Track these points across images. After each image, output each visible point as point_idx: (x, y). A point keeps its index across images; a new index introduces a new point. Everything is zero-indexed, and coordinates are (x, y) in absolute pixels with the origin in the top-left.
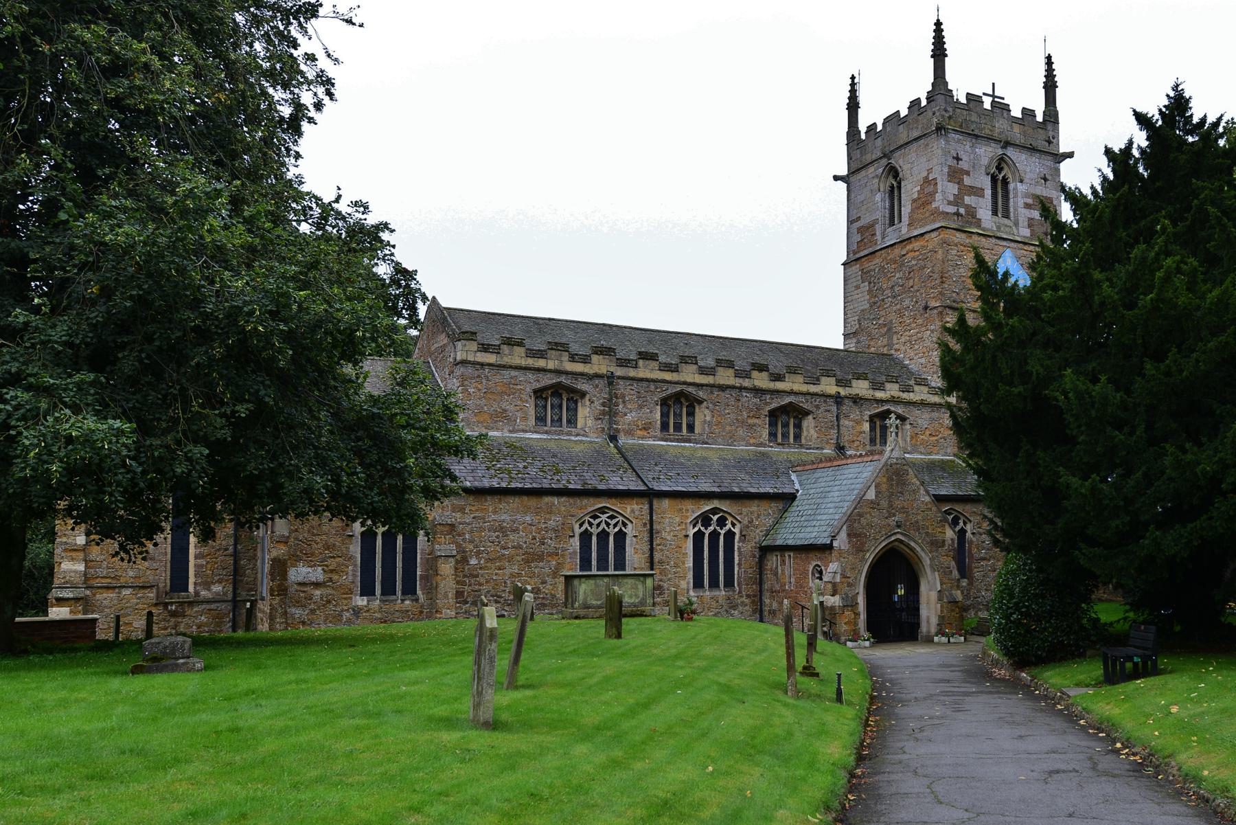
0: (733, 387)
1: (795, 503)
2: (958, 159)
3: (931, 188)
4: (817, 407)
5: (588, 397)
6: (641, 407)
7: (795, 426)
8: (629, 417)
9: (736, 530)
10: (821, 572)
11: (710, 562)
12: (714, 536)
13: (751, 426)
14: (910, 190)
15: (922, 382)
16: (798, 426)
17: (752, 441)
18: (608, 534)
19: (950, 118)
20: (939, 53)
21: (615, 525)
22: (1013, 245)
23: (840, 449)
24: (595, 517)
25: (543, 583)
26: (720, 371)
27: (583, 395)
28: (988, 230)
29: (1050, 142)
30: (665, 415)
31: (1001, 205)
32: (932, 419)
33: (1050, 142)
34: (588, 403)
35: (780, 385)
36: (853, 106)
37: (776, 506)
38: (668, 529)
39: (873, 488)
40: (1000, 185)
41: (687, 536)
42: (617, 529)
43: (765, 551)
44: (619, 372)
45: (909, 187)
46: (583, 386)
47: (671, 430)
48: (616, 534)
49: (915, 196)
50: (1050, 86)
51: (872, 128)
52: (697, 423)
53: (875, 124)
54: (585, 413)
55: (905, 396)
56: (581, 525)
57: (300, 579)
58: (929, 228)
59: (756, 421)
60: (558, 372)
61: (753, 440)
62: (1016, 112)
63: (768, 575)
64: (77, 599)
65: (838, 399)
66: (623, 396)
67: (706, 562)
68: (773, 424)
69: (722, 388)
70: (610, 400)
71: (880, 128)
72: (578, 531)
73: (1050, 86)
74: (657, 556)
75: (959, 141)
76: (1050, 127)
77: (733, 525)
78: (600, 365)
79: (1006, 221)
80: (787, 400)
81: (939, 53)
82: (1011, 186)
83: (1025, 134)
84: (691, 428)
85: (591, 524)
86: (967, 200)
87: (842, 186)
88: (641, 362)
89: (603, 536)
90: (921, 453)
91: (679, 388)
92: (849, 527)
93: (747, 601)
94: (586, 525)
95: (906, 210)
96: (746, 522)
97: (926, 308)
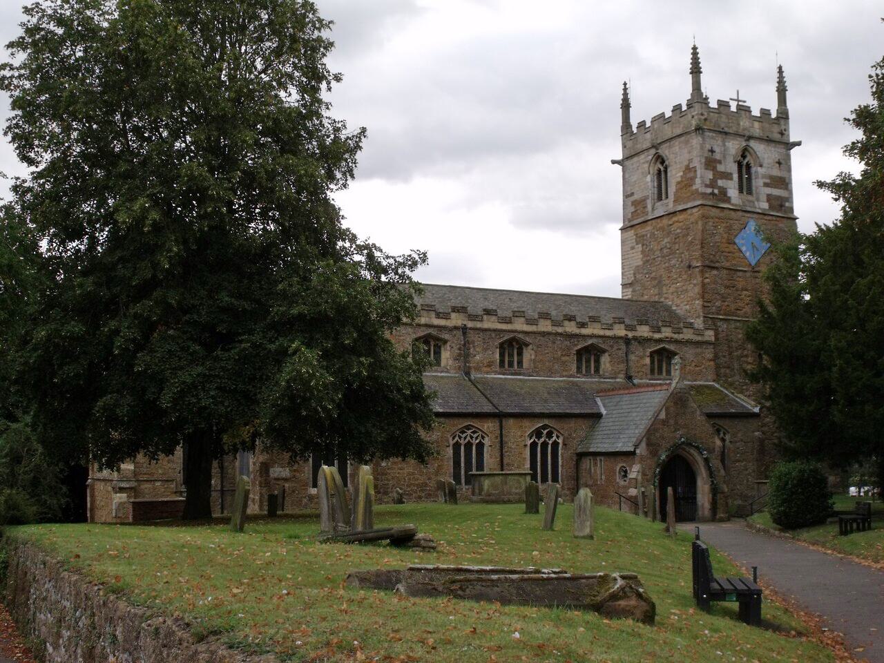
0: (549, 334)
1: (602, 421)
2: (712, 151)
3: (692, 174)
4: (612, 347)
5: (449, 344)
6: (485, 350)
7: (595, 361)
8: (478, 357)
9: (560, 441)
10: (626, 472)
11: (541, 465)
12: (545, 445)
13: (564, 363)
14: (675, 175)
15: (690, 326)
16: (597, 362)
17: (565, 373)
18: (472, 444)
19: (706, 120)
20: (696, 70)
21: (477, 438)
22: (755, 216)
23: (629, 378)
24: (463, 432)
25: (429, 479)
26: (542, 322)
27: (445, 342)
28: (736, 205)
29: (782, 134)
30: (502, 355)
31: (746, 186)
32: (697, 355)
33: (782, 134)
34: (449, 348)
35: (585, 331)
36: (626, 105)
37: (588, 422)
38: (513, 440)
39: (664, 410)
40: (744, 168)
41: (526, 446)
42: (477, 441)
43: (581, 456)
44: (470, 324)
45: (674, 172)
46: (446, 336)
47: (516, 367)
48: (477, 444)
49: (679, 179)
50: (782, 91)
51: (642, 125)
52: (524, 360)
53: (644, 121)
54: (446, 355)
55: (676, 336)
56: (453, 438)
57: (276, 475)
58: (689, 205)
59: (567, 358)
60: (427, 326)
61: (566, 376)
62: (756, 112)
63: (583, 474)
64: (131, 488)
65: (627, 341)
66: (473, 342)
67: (539, 464)
68: (579, 360)
69: (544, 334)
70: (464, 345)
71: (648, 124)
72: (452, 443)
73: (782, 91)
74: (506, 461)
75: (713, 138)
76: (782, 122)
77: (558, 437)
78: (456, 320)
79: (750, 198)
80: (590, 342)
81: (696, 70)
82: (753, 170)
83: (762, 129)
84: (520, 363)
85: (460, 437)
86: (720, 183)
87: (619, 168)
88: (485, 317)
89: (468, 446)
90: (689, 380)
91: (512, 335)
92: (648, 439)
93: (568, 493)
94: (457, 438)
95: (672, 189)
96: (566, 435)
97: (689, 267)
